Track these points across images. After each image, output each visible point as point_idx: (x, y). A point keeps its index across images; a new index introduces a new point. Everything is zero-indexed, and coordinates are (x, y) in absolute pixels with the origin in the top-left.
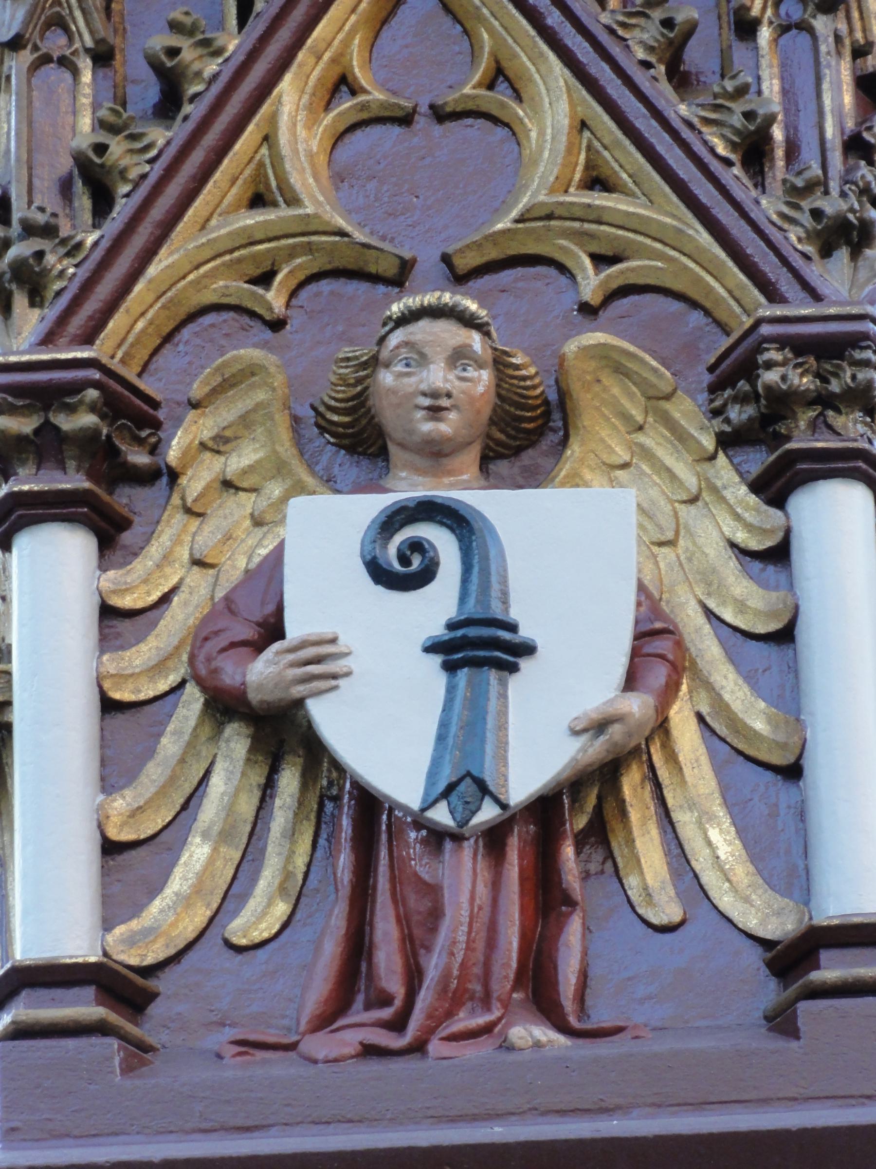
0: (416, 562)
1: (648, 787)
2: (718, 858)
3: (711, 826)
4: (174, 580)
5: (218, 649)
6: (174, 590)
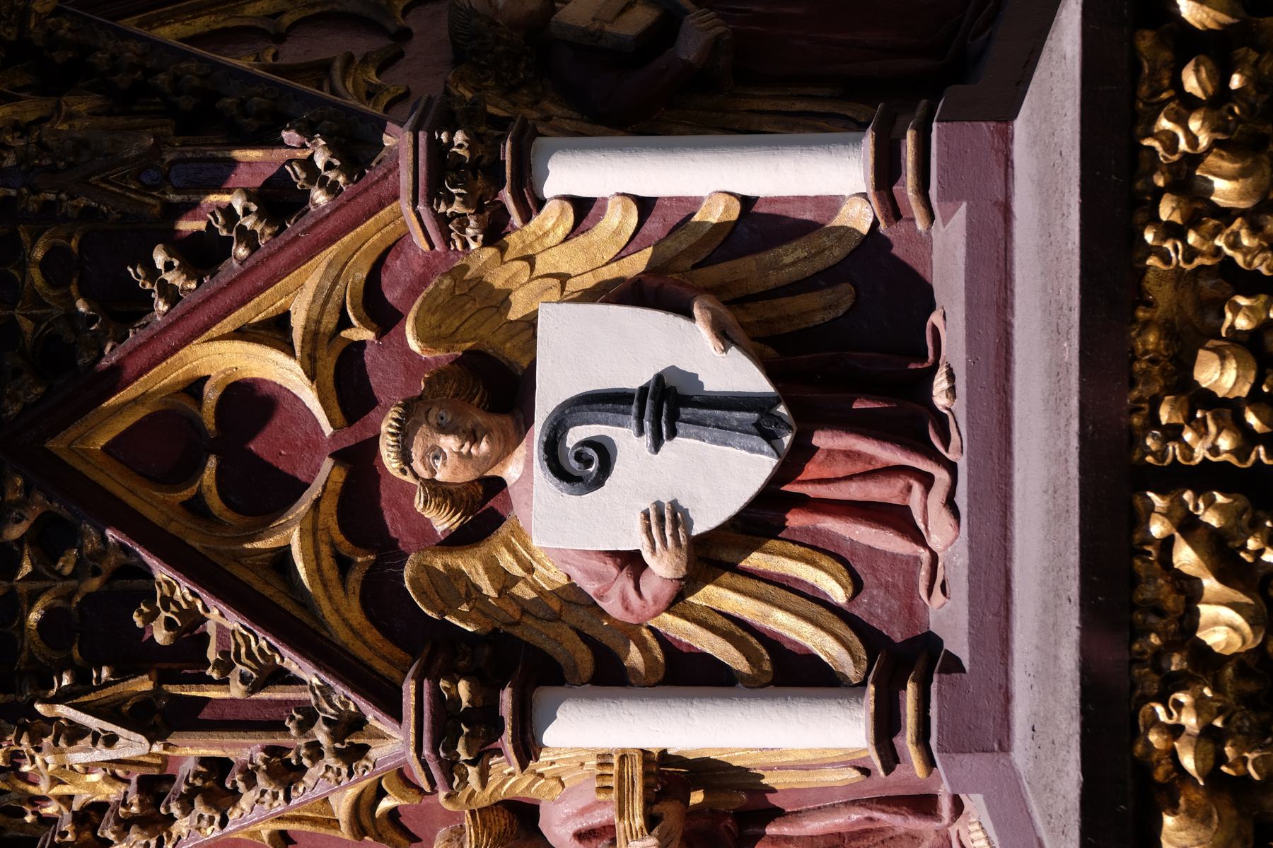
0: (591, 452)
1: (748, 305)
2: (806, 257)
3: (781, 261)
4: (571, 633)
5: (639, 599)
6: (579, 632)
